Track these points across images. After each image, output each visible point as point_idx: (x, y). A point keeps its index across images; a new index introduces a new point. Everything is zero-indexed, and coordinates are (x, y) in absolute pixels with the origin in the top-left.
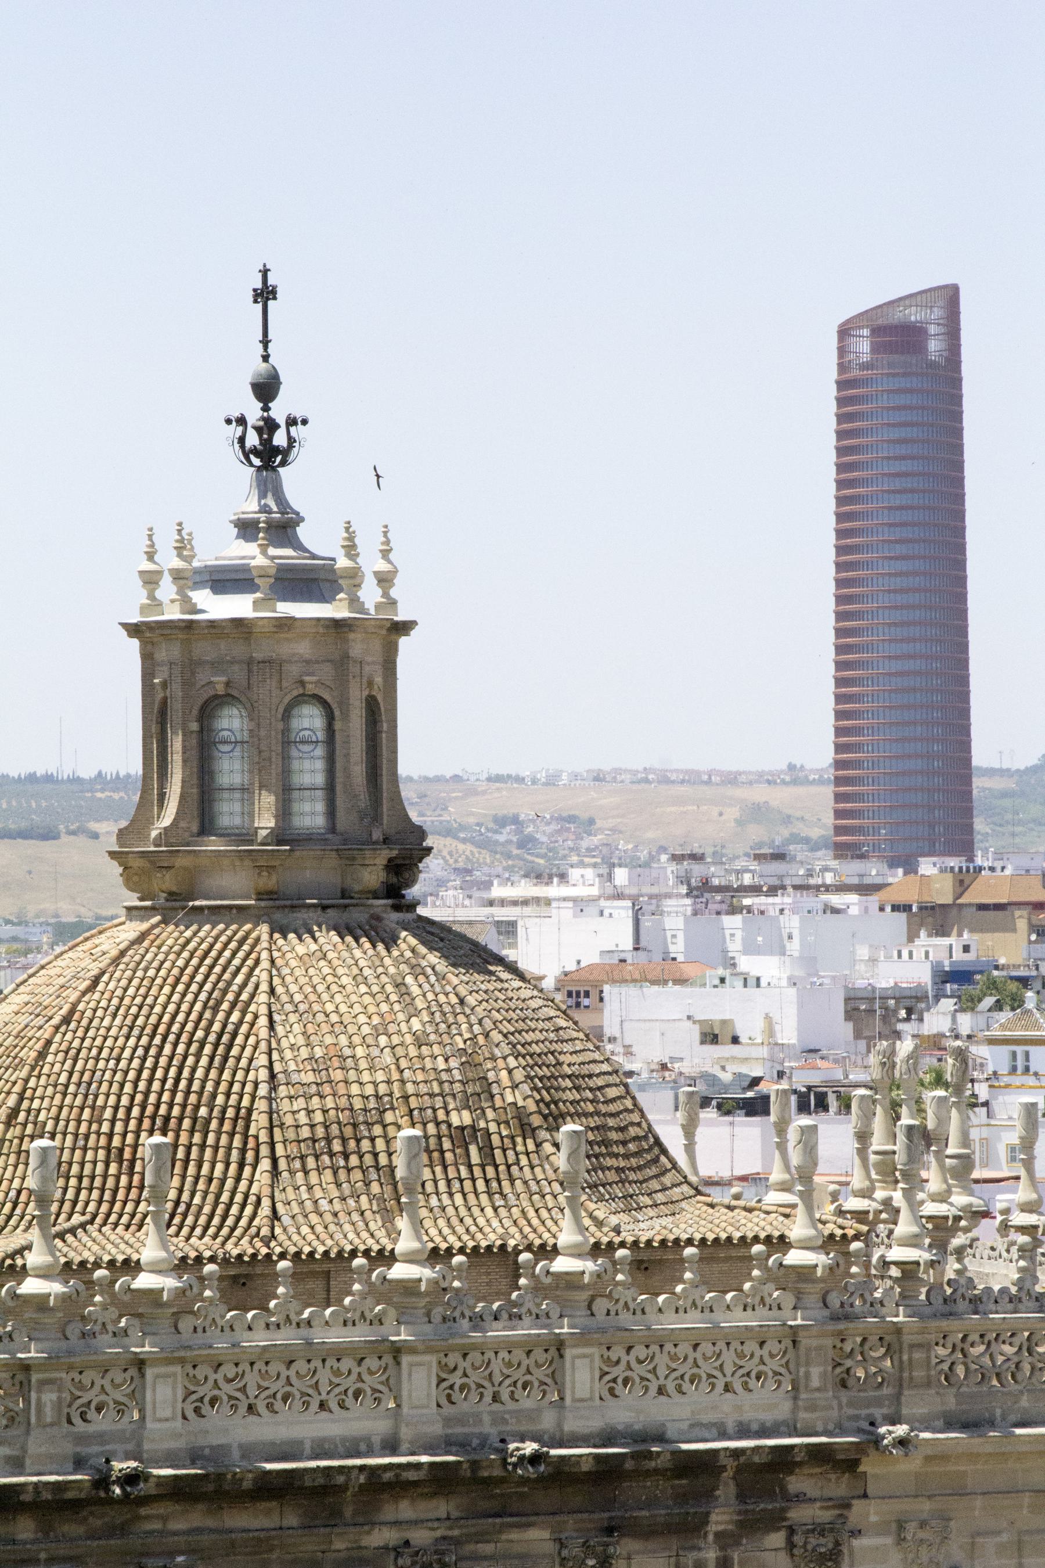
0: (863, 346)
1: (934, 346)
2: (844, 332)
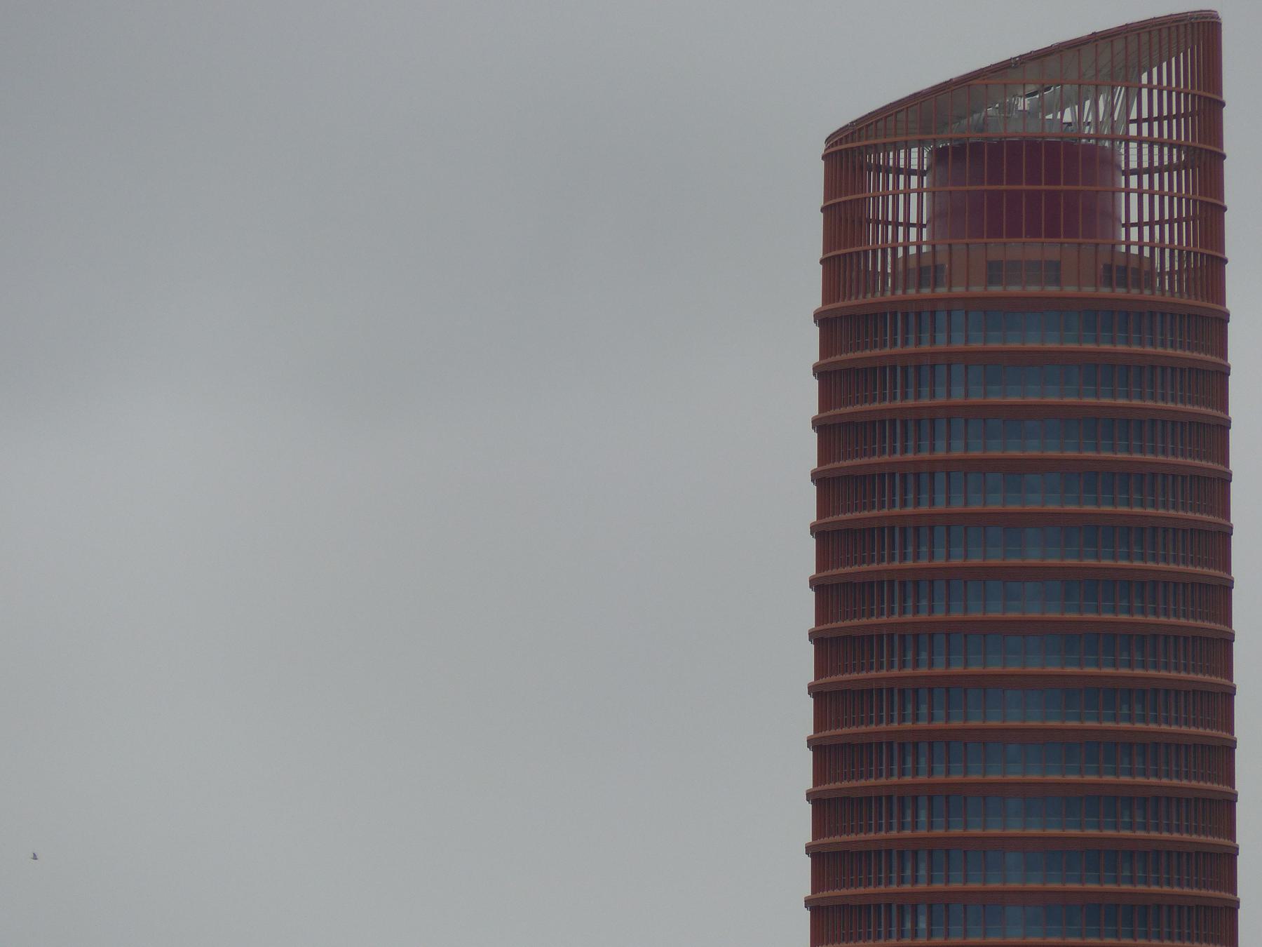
0: (910, 207)
1: (1140, 214)
2: (853, 158)
